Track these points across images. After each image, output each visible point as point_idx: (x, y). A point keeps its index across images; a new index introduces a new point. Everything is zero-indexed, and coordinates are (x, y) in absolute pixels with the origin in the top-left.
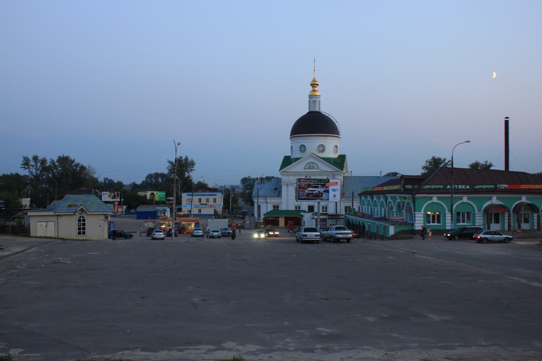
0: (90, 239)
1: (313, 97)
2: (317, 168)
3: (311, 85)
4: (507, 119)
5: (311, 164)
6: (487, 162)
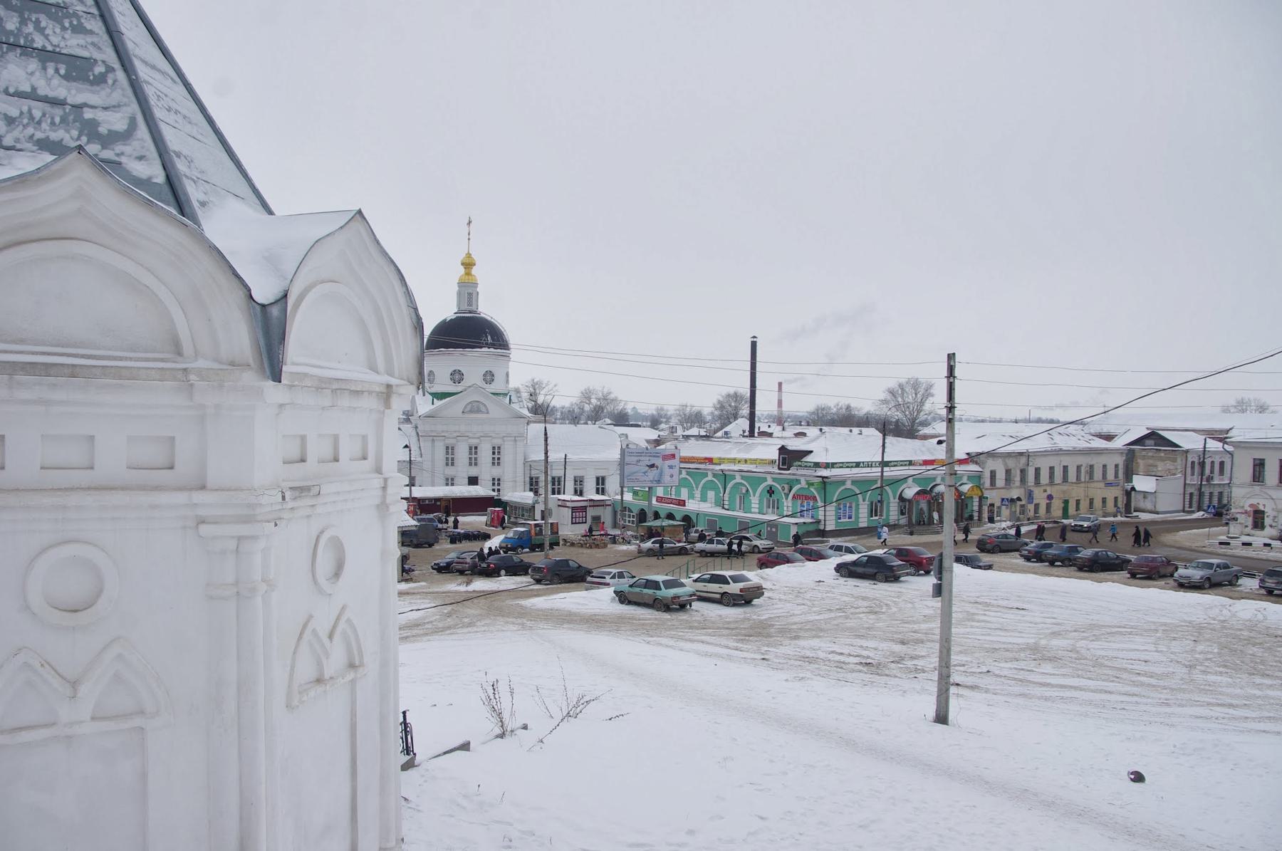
1: (468, 286)
3: (462, 264)
4: (755, 340)
5: (475, 404)
6: (610, 393)
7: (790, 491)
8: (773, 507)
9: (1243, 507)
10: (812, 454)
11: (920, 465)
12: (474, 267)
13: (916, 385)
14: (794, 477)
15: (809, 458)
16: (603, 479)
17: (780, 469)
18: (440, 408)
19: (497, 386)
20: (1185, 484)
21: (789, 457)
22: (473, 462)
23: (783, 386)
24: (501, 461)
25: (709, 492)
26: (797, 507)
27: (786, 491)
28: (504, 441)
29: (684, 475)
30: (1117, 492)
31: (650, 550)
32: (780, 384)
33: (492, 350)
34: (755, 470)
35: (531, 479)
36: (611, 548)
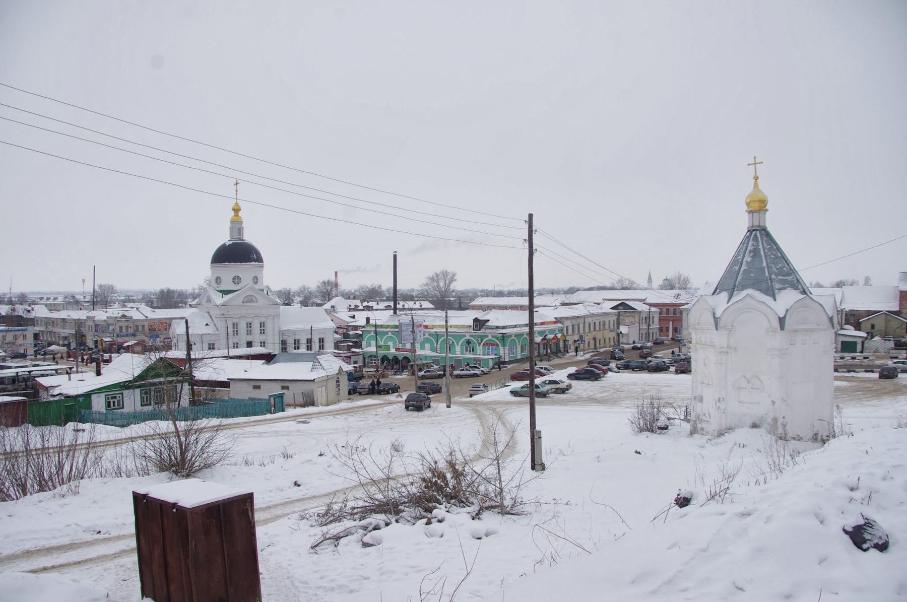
0: (717, 283)
3: (233, 210)
7: (482, 341)
8: (470, 351)
9: (688, 339)
10: (490, 321)
11: (540, 325)
12: (240, 211)
13: (445, 274)
14: (484, 334)
15: (489, 324)
16: (323, 339)
17: (474, 330)
18: (230, 300)
20: (640, 329)
21: (479, 324)
22: (249, 333)
24: (265, 331)
25: (426, 344)
26: (486, 350)
27: (480, 341)
29: (427, 336)
30: (613, 335)
31: (423, 376)
32: (336, 273)
33: (257, 263)
34: (458, 331)
35: (282, 341)
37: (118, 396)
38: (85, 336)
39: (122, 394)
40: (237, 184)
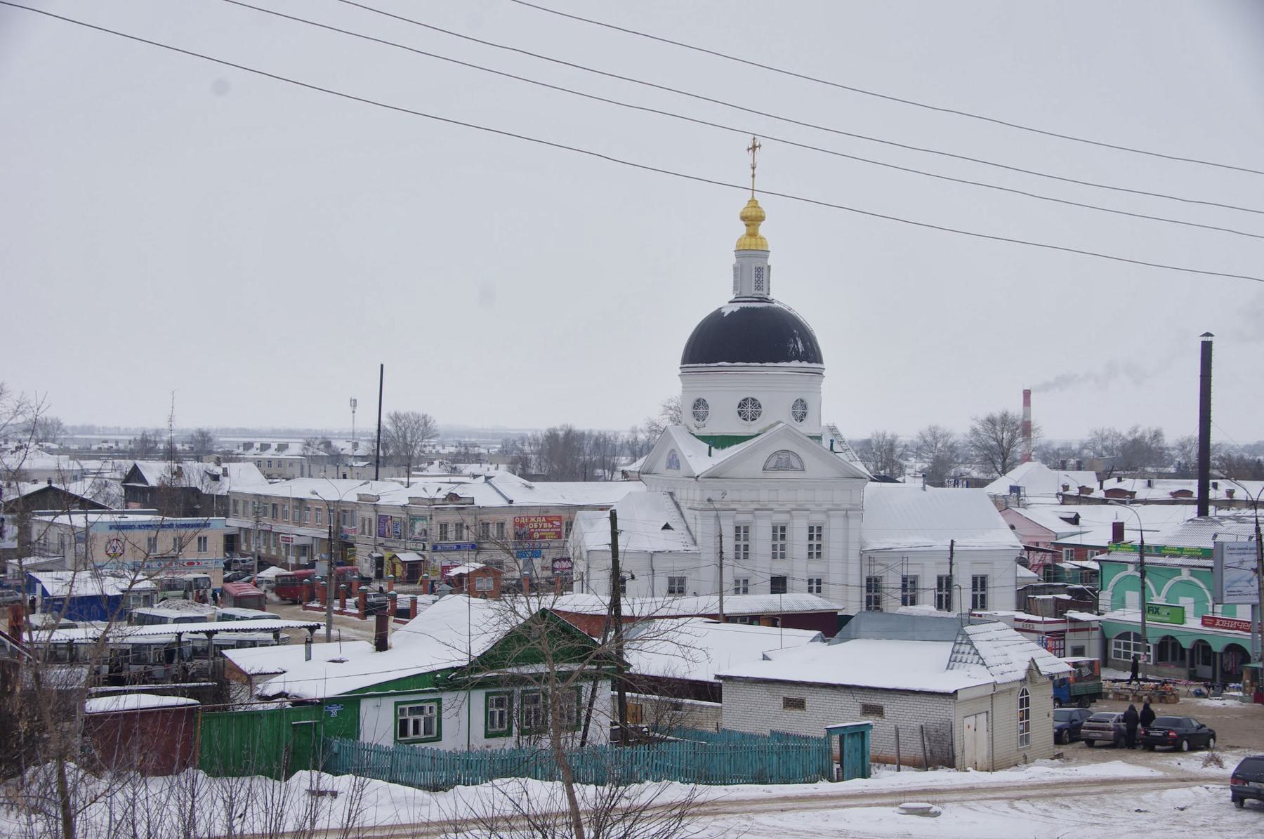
1: (756, 257)
2: (799, 467)
3: (743, 218)
5: (784, 457)
12: (763, 223)
19: (806, 428)
22: (779, 553)
23: (1033, 396)
24: (823, 551)
28: (828, 516)
32: (1027, 394)
33: (805, 364)
36: (1185, 703)
37: (427, 706)
38: (352, 545)
39: (439, 701)
40: (754, 147)
